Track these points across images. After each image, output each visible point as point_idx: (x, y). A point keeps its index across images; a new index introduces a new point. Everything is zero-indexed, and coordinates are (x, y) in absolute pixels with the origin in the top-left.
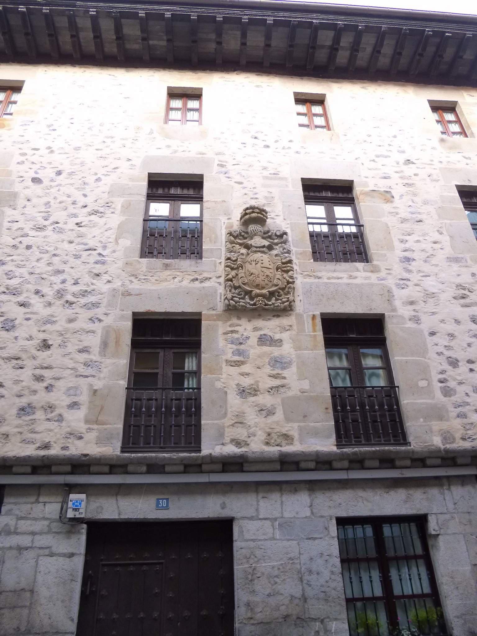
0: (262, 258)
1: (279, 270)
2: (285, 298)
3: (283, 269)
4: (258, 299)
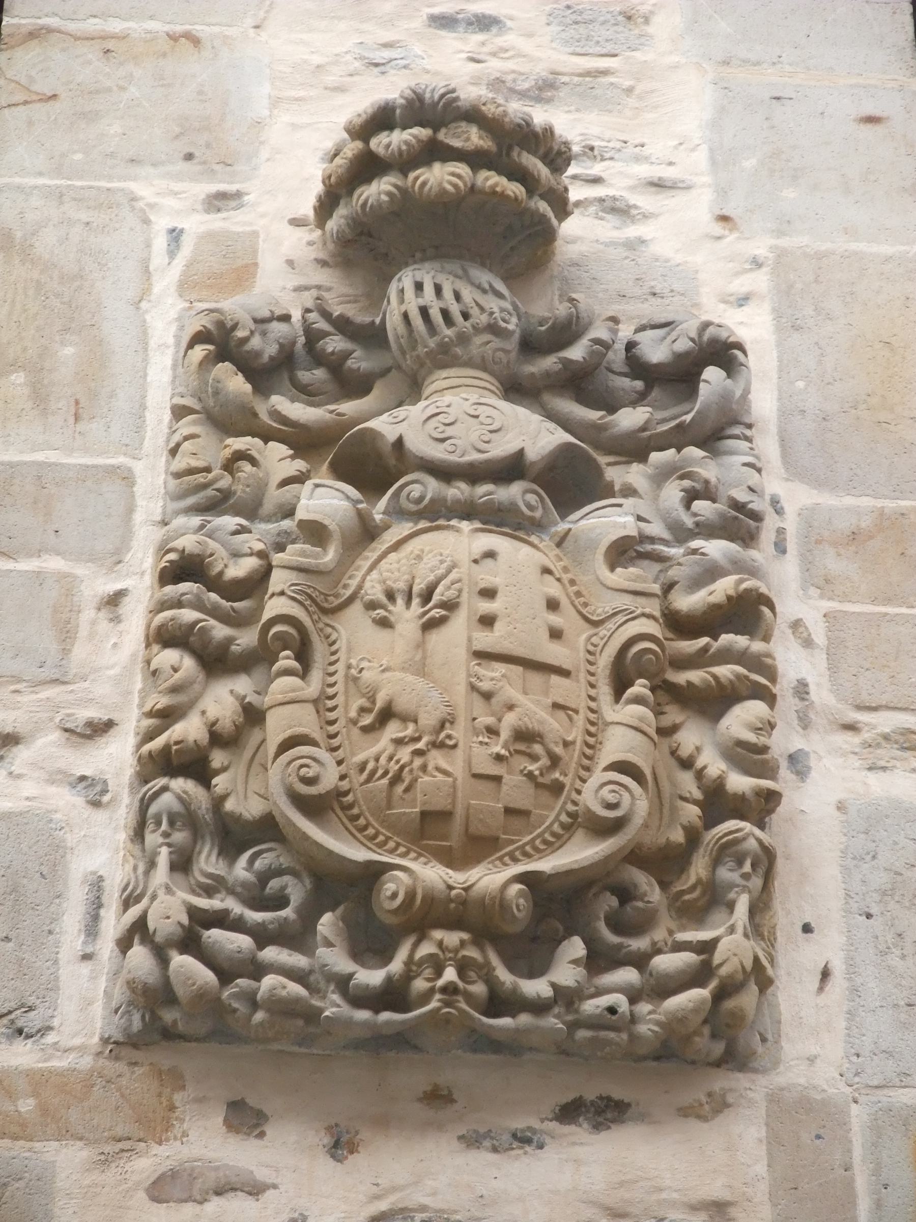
0: (486, 576)
1: (640, 687)
2: (679, 947)
3: (682, 678)
4: (426, 949)
